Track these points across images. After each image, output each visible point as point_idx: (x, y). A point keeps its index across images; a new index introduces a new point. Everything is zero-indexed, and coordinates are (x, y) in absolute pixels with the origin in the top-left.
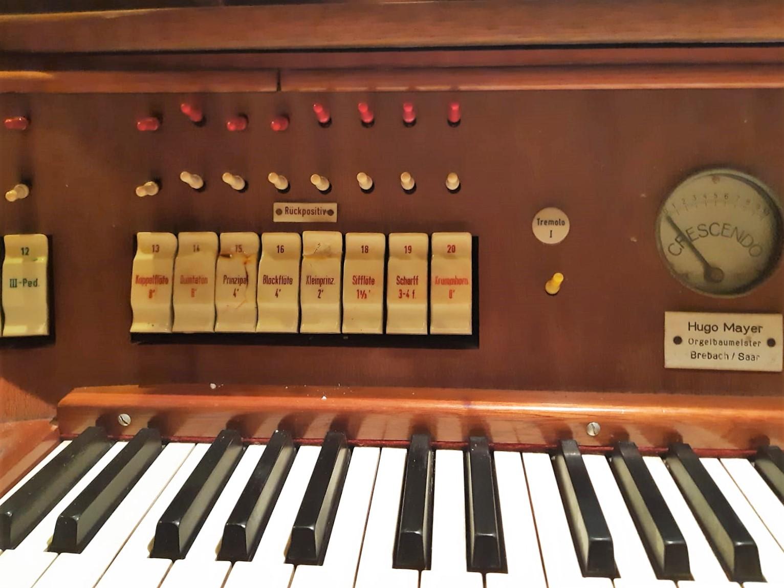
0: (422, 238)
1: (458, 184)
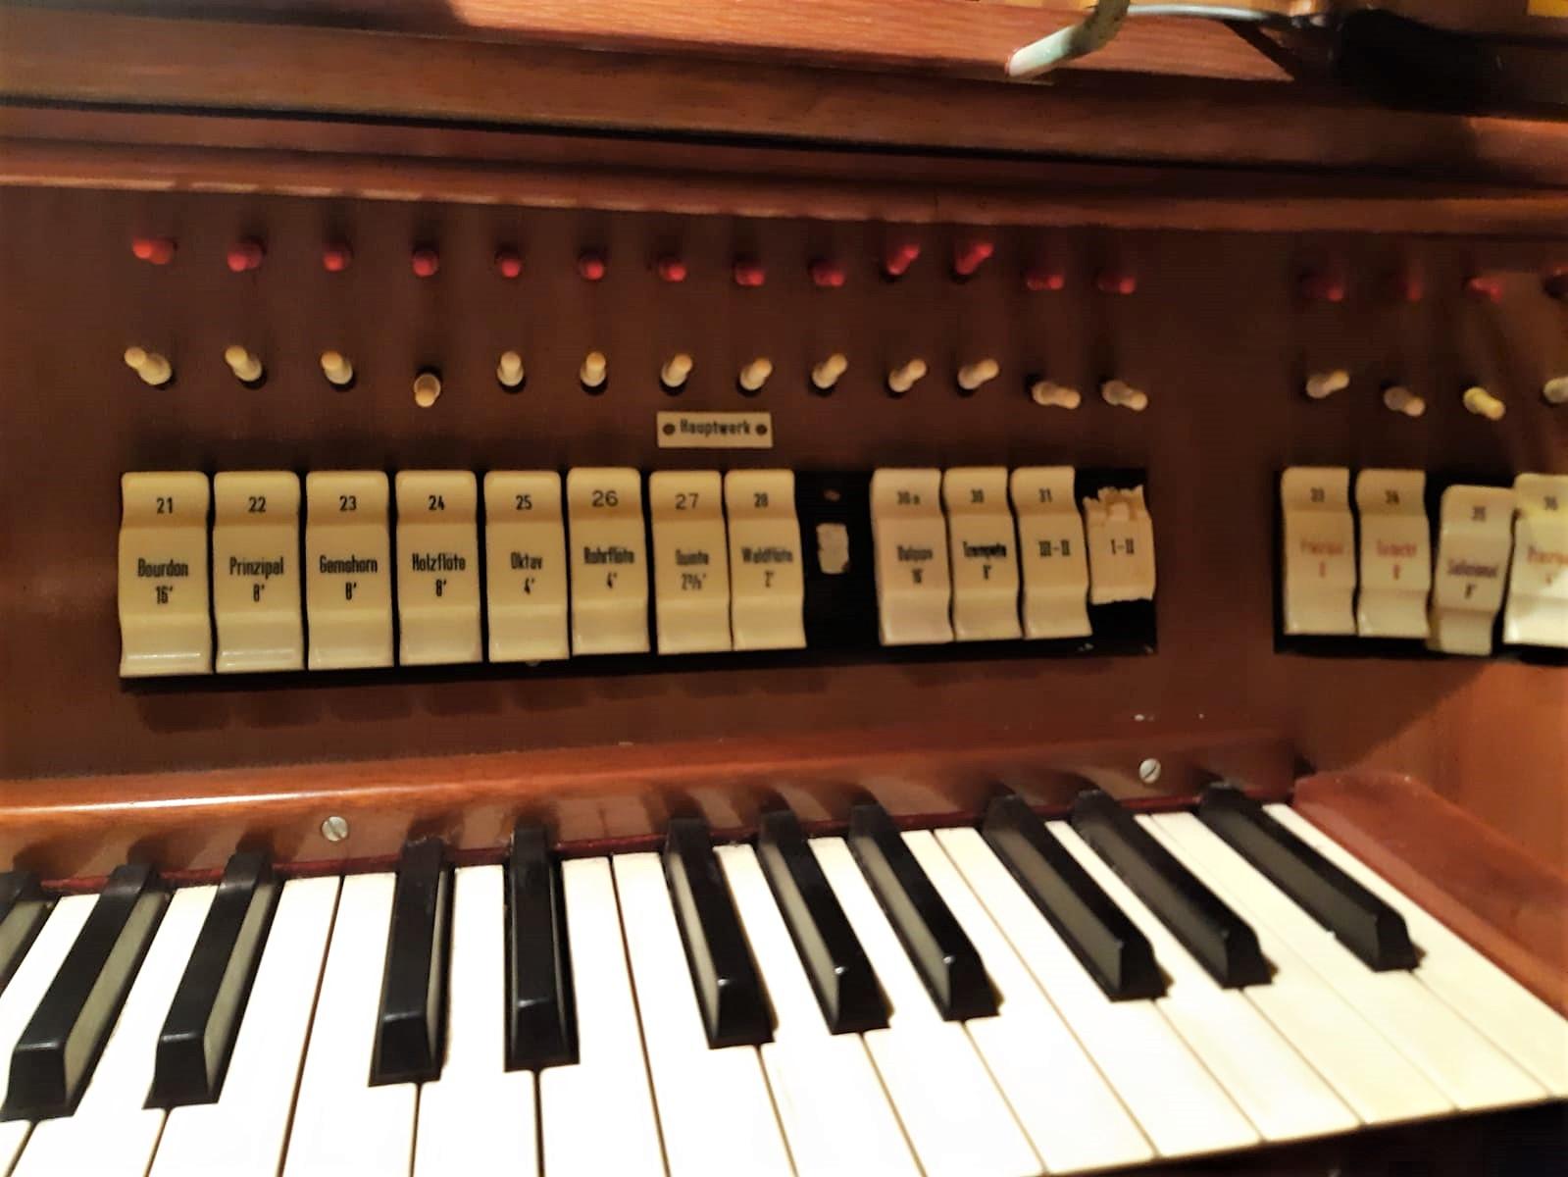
0: (1341, 476)
1: (603, 378)
